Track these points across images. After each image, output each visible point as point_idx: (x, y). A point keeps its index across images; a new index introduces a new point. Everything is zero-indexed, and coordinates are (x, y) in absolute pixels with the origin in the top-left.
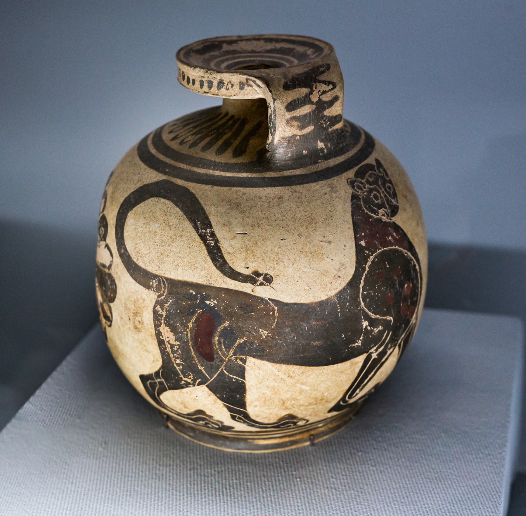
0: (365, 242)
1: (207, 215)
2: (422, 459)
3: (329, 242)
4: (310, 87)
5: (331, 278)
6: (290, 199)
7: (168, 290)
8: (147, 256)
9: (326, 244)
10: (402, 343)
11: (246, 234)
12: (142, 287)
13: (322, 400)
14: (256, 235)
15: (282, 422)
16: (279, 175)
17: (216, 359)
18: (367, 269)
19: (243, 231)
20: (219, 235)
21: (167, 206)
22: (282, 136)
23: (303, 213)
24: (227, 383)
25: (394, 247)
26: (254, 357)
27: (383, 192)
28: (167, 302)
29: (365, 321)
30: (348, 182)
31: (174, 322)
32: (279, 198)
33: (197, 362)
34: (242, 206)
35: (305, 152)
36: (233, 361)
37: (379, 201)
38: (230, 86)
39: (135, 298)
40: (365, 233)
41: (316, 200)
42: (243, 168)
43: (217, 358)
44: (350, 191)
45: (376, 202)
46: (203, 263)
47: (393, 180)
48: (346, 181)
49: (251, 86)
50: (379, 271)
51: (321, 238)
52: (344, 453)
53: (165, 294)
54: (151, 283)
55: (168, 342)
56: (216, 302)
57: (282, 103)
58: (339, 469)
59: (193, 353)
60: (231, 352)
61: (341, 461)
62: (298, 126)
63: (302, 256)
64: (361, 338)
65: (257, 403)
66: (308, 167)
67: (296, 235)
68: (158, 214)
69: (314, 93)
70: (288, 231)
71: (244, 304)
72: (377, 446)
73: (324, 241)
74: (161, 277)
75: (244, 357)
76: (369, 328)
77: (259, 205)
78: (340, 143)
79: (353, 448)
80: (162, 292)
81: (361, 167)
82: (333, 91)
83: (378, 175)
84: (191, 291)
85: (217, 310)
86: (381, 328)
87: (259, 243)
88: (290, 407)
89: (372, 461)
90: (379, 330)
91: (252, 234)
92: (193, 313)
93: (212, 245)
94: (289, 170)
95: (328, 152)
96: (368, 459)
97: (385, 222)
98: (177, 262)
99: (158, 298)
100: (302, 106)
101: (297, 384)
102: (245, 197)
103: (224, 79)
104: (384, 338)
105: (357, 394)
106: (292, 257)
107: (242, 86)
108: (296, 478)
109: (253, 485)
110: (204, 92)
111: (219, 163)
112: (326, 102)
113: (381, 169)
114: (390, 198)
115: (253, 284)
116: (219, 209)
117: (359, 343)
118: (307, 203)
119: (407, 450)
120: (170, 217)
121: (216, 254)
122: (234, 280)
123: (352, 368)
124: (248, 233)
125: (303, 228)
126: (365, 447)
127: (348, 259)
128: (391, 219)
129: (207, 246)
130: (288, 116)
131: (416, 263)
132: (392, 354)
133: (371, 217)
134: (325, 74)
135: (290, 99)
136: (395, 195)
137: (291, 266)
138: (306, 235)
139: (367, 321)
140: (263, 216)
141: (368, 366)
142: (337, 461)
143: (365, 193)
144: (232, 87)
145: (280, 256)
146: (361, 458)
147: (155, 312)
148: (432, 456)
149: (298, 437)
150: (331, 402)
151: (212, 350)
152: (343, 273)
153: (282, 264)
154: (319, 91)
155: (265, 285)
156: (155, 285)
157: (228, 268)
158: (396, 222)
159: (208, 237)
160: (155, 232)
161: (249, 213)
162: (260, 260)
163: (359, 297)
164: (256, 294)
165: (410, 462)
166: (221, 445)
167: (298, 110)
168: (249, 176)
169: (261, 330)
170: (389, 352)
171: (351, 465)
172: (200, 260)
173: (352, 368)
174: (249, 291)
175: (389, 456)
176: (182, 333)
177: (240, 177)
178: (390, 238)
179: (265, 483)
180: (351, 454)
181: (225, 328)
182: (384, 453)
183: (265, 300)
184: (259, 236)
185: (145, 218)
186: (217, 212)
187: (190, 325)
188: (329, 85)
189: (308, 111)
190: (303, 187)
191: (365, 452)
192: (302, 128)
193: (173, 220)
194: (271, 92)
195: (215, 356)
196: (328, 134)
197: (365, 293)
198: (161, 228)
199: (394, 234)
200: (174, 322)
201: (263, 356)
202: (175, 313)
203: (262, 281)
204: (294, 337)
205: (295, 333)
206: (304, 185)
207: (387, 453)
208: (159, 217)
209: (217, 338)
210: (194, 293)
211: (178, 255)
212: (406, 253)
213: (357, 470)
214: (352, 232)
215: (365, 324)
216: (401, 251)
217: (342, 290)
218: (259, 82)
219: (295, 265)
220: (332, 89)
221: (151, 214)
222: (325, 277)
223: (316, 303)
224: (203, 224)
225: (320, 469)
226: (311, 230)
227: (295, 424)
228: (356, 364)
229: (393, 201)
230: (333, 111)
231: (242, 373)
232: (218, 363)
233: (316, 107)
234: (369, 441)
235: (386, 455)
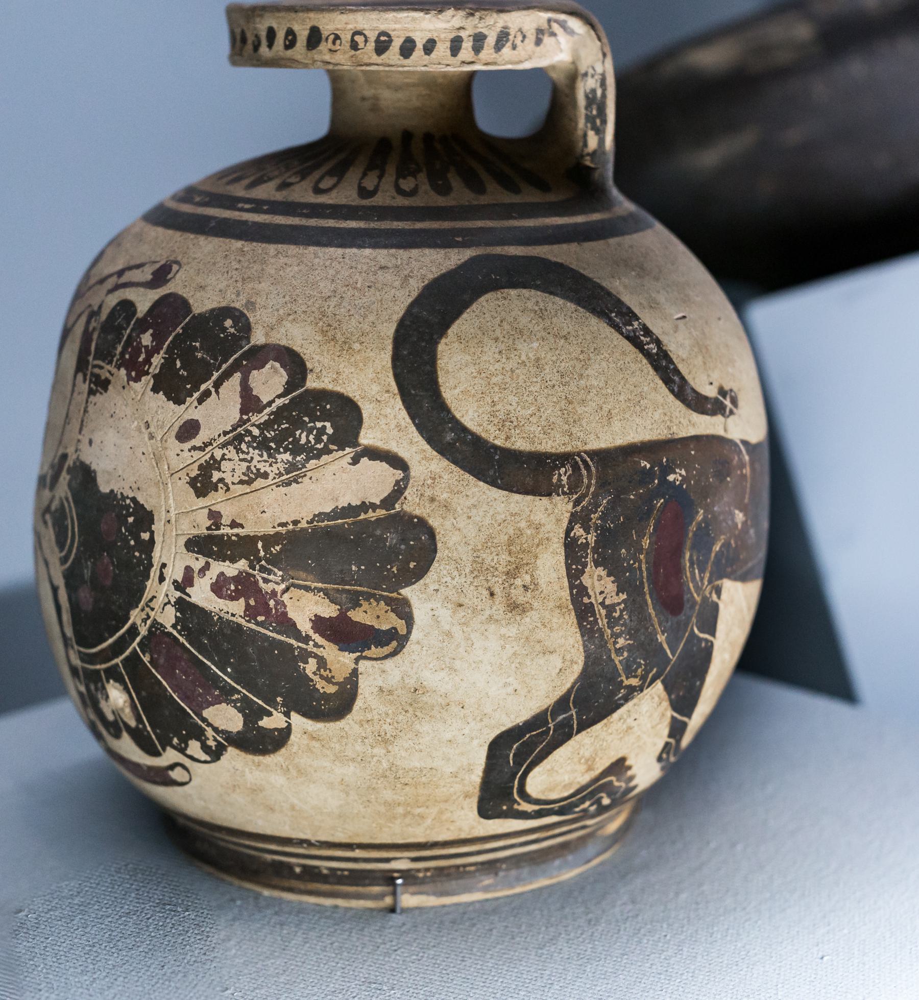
7: (598, 478)
8: (534, 420)
12: (529, 498)
20: (656, 330)
21: (534, 300)
28: (597, 506)
38: (520, 38)
39: (511, 532)
40: (134, 546)
46: (653, 394)
53: (592, 489)
54: (555, 479)
55: (602, 604)
59: (651, 611)
68: (524, 320)
74: (579, 455)
80: (583, 490)
98: (606, 408)
99: (574, 506)
103: (510, 25)
110: (463, 62)
120: (554, 320)
129: (647, 354)
144: (522, 41)
156: (564, 478)
159: (642, 338)
160: (538, 360)
172: (646, 389)
185: (496, 339)
187: (646, 543)
198: (547, 348)
208: (530, 326)
210: (648, 466)
211: (604, 392)
221: (506, 326)
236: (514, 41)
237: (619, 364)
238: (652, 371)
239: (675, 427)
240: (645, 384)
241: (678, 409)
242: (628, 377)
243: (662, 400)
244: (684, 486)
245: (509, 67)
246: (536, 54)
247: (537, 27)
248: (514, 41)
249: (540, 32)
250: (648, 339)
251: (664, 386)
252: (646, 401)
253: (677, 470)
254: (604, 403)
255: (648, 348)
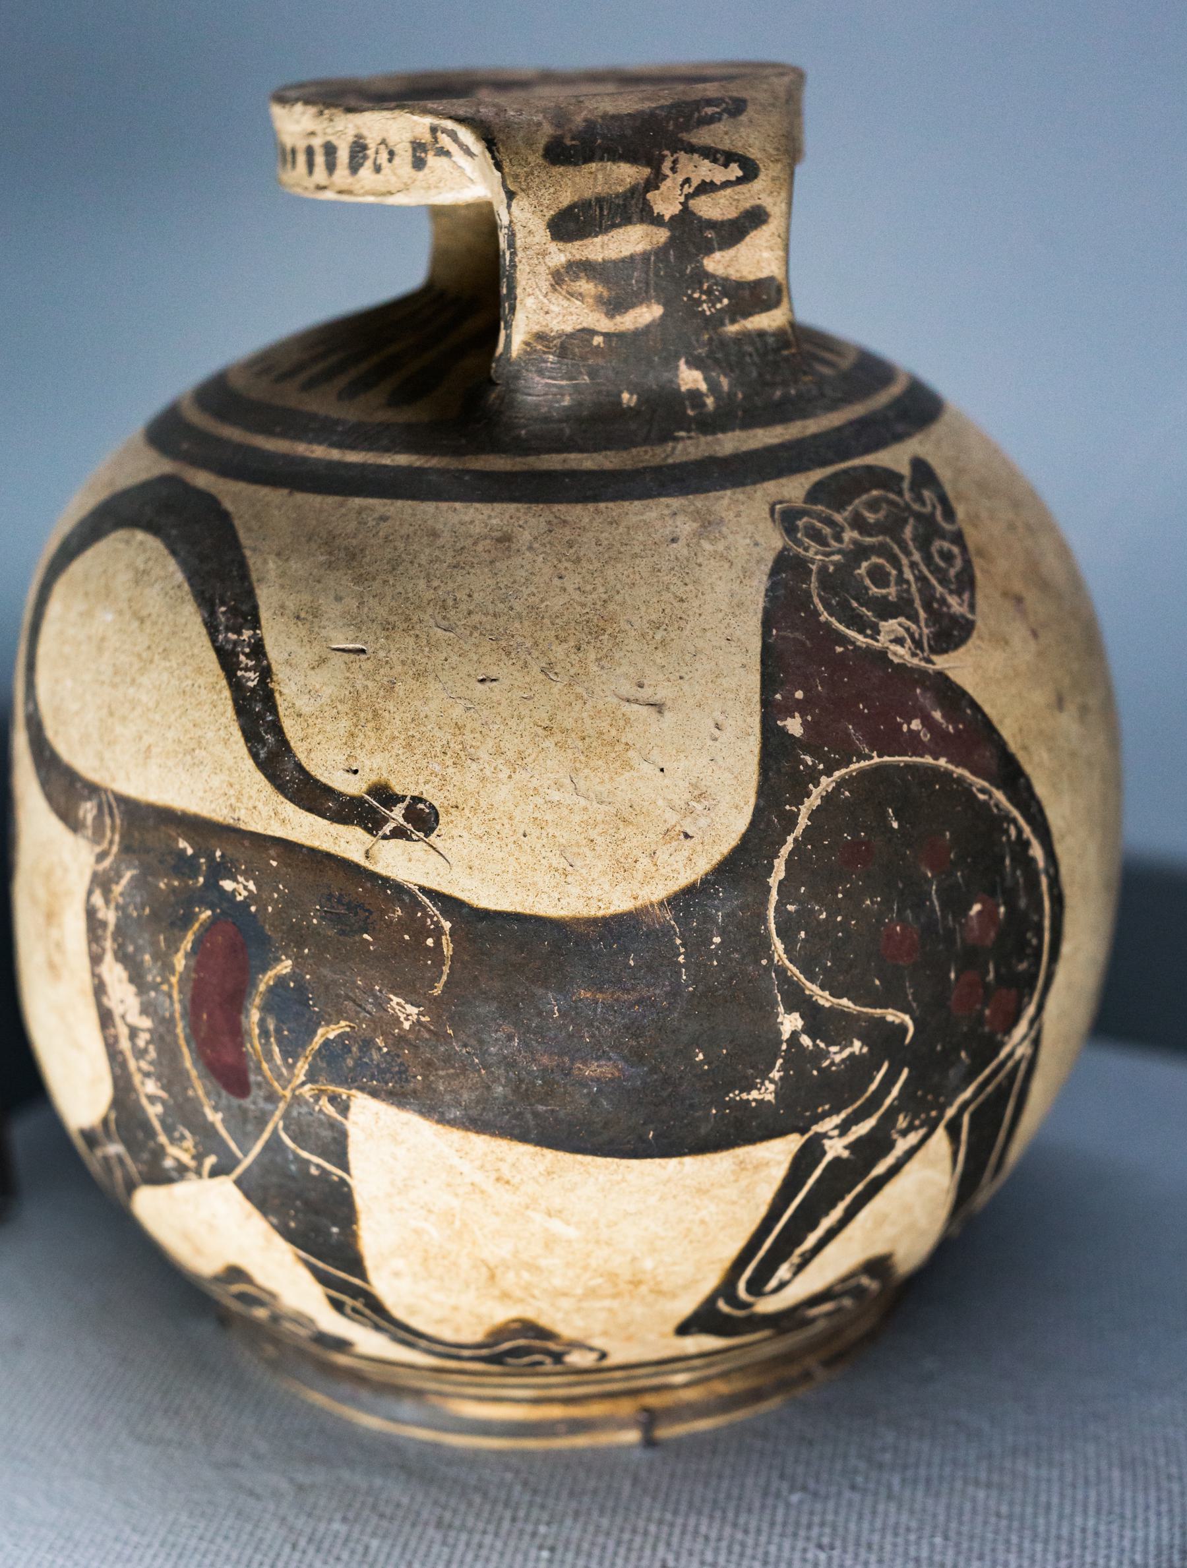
0: (805, 724)
1: (251, 584)
2: (1008, 1551)
3: (658, 707)
4: (648, 164)
5: (652, 836)
6: (536, 545)
7: (122, 837)
9: (645, 710)
10: (966, 1119)
11: (363, 651)
13: (636, 1283)
14: (394, 656)
15: (507, 1345)
16: (518, 468)
17: (255, 1091)
18: (803, 822)
19: (354, 641)
22: (536, 328)
23: (576, 596)
24: (293, 1178)
25: (928, 760)
26: (374, 1094)
27: (913, 565)
28: (119, 876)
29: (789, 1010)
30: (772, 511)
31: (138, 949)
32: (499, 540)
33: (201, 1092)
34: (367, 559)
35: (627, 398)
36: (307, 1103)
37: (892, 592)
38: (384, 156)
41: (635, 556)
42: (413, 440)
43: (259, 1085)
44: (775, 541)
45: (875, 591)
47: (972, 537)
48: (767, 508)
49: (447, 154)
50: (855, 834)
51: (628, 689)
52: (742, 1486)
56: (251, 885)
57: (537, 207)
58: (701, 1540)
59: (188, 1063)
60: (302, 1068)
61: (718, 1514)
62: (599, 300)
63: (549, 743)
64: (776, 1074)
65: (398, 1263)
66: (634, 451)
67: (535, 669)
69: (664, 186)
70: (508, 654)
71: (339, 901)
72: (867, 1479)
73: (636, 701)
75: (343, 1092)
76: (806, 1041)
77: (423, 559)
78: (773, 385)
79: (782, 1476)
81: (845, 472)
82: (739, 188)
83: (908, 507)
84: (182, 844)
85: (254, 915)
86: (857, 1046)
87: (400, 688)
88: (518, 1293)
89: (827, 1530)
90: (852, 1055)
91: (382, 654)
92: (187, 920)
93: (251, 684)
94: (559, 451)
95: (718, 407)
96: (816, 1519)
97: (902, 667)
98: (147, 740)
100: (614, 226)
101: (529, 1213)
102: (384, 528)
103: (365, 132)
104: (873, 1087)
105: (782, 1285)
106: (511, 745)
107: (419, 154)
108: (541, 1548)
109: (386, 1549)
111: (337, 422)
112: (712, 224)
113: (927, 494)
114: (939, 589)
115: (369, 831)
116: (295, 565)
117: (766, 1093)
118: (597, 565)
119: (968, 1506)
121: (260, 716)
122: (310, 810)
123: (743, 1183)
124: (370, 651)
125: (565, 646)
126: (825, 1476)
127: (727, 775)
128: (929, 661)
129: (236, 686)
130: (559, 255)
131: (1027, 831)
132: (920, 1155)
133: (843, 640)
134: (719, 127)
135: (566, 198)
136: (966, 583)
137: (503, 776)
138: (572, 672)
139: (796, 1015)
140: (429, 594)
141: (811, 1181)
142: (706, 1510)
143: (836, 558)
144: (390, 160)
145: (468, 737)
146: (793, 1513)
147: (91, 913)
148: (1046, 1542)
149: (596, 1410)
150: (673, 1295)
151: (243, 1056)
152: (703, 822)
153: (474, 766)
154: (687, 181)
155: (409, 839)
157: (291, 766)
158: (951, 674)
159: (242, 658)
160: (103, 639)
161: (385, 582)
162: (397, 748)
163: (765, 920)
164: (380, 868)
165: (958, 1553)
166: (342, 1400)
167: (598, 240)
168: (418, 464)
169: (395, 999)
170: (902, 1145)
171: (746, 1532)
172: (210, 735)
173: (743, 1183)
174: (355, 855)
175: (892, 1521)
176: (156, 987)
177: (386, 466)
178: (916, 725)
179: (430, 1547)
180: (765, 1494)
181: (281, 981)
182: (881, 1508)
183: (409, 892)
184: (403, 663)
186: (283, 575)
188: (726, 166)
189: (640, 248)
190: (597, 511)
191: (815, 1495)
192: (615, 306)
193: (153, 599)
194: (498, 166)
195: (253, 1078)
196: (723, 343)
197: (791, 908)
199: (937, 715)
200: (138, 949)
201: (404, 1095)
202: (139, 916)
203: (401, 821)
204: (510, 1038)
205: (515, 1024)
206: (602, 505)
207: (893, 1508)
209: (255, 1015)
210: (190, 851)
212: (983, 791)
213: (760, 1551)
214: (754, 680)
215: (790, 1023)
216: (961, 780)
217: (693, 885)
218: (466, 136)
219: (521, 776)
220: (739, 181)
222: (630, 830)
223: (593, 922)
224: (233, 612)
225: (634, 1531)
226: (592, 656)
227: (558, 1358)
228: (757, 1168)
229: (953, 600)
230: (742, 259)
231: (337, 1149)
232: (262, 1104)
233: (672, 239)
234: (845, 1457)
235: (886, 1515)
236: (375, 159)
237: (184, 684)
238: (230, 712)
239: (243, 811)
240: (212, 727)
241: (257, 787)
242: (189, 707)
243: (231, 762)
244: (253, 909)
245: (371, 199)
246: (417, 183)
247: (411, 139)
248: (375, 159)
249: (418, 147)
250: (251, 663)
251: (242, 741)
252: (203, 753)
253: (241, 879)
254: (146, 732)
255: (243, 676)
